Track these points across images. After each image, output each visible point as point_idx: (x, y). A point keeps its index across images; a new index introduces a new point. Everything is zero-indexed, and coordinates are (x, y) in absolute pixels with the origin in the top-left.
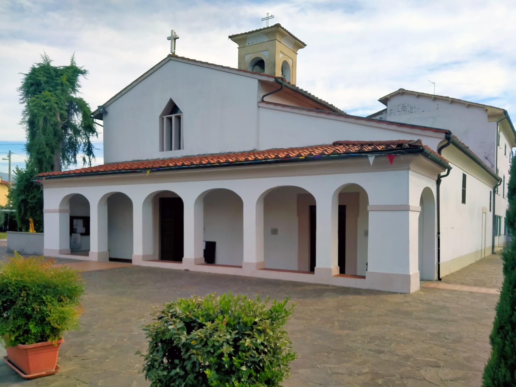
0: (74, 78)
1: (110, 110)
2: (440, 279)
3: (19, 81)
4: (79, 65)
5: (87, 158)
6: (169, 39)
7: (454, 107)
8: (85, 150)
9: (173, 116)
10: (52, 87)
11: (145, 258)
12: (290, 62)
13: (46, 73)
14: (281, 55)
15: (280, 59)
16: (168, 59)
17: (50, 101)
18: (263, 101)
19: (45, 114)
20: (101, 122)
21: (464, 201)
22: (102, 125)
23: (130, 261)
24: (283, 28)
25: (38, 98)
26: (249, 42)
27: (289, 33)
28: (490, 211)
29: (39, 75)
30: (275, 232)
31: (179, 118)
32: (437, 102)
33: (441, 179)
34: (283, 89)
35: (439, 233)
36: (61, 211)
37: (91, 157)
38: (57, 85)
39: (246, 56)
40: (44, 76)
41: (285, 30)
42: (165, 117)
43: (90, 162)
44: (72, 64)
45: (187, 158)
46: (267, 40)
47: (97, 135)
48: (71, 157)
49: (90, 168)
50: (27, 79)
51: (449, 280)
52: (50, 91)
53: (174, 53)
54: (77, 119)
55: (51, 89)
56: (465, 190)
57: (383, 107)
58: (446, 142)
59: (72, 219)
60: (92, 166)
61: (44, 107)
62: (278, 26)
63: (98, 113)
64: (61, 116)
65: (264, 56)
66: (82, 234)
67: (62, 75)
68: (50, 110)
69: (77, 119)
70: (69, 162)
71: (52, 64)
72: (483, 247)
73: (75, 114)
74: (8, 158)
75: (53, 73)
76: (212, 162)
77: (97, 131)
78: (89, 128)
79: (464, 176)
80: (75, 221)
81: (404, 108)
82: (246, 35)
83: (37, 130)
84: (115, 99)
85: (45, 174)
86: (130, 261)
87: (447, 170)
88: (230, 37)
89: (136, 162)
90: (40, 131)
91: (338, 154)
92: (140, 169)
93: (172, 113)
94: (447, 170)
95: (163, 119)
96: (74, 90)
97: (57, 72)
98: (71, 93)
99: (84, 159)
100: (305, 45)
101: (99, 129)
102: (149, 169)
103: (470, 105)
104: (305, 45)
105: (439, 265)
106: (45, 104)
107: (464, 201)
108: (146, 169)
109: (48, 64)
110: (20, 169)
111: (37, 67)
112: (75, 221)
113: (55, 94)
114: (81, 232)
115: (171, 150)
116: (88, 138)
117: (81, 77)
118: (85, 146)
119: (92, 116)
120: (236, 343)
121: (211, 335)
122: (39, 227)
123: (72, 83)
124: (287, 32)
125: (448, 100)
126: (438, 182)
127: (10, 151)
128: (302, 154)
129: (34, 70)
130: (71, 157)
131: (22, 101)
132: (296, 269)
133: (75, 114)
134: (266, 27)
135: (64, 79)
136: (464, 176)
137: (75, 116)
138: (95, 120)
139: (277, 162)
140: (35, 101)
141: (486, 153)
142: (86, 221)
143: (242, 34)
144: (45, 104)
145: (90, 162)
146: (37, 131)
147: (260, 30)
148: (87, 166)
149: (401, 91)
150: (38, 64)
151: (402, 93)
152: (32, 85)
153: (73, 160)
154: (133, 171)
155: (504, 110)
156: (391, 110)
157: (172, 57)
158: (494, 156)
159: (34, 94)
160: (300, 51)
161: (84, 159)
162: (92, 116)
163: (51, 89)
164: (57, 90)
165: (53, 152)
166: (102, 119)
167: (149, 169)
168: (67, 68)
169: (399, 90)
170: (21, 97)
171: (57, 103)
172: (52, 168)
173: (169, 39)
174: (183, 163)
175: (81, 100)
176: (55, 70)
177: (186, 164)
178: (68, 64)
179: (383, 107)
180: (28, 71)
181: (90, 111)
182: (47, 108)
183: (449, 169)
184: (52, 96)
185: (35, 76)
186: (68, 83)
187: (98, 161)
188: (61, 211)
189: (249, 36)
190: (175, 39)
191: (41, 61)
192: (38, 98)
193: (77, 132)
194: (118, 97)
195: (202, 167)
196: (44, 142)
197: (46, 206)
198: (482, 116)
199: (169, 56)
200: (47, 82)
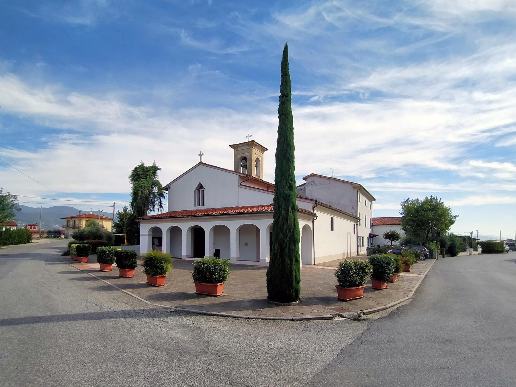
0: (155, 172)
1: (171, 186)
2: (315, 264)
3: (130, 173)
4: (157, 165)
5: (160, 209)
6: (199, 155)
7: (337, 183)
8: (159, 205)
9: (201, 190)
10: (145, 176)
11: (188, 256)
12: (260, 158)
13: (142, 170)
14: (255, 155)
15: (254, 157)
16: (199, 164)
17: (144, 184)
18: (241, 185)
19: (142, 189)
20: (167, 192)
21: (332, 229)
22: (168, 193)
23: (181, 258)
24: (256, 142)
25: (138, 182)
26: (239, 148)
27: (259, 144)
28: (354, 234)
29: (139, 171)
30: (246, 244)
31: (203, 191)
32: (329, 180)
33: (314, 220)
34: (250, 179)
35: (314, 244)
36: (148, 235)
37: (162, 208)
38: (147, 175)
39: (238, 155)
40: (141, 171)
41: (257, 143)
42: (197, 191)
43: (161, 211)
44: (154, 165)
45: (207, 210)
46: (248, 148)
47: (165, 198)
48: (152, 208)
49: (162, 214)
50: (133, 173)
51: (318, 265)
52: (144, 179)
53: (201, 162)
54: (155, 190)
55: (145, 177)
56: (333, 225)
57: (305, 182)
58: (316, 205)
59: (153, 238)
60: (162, 213)
61: (141, 186)
62: (253, 141)
63: (166, 188)
64: (149, 190)
65: (247, 155)
66: (157, 246)
67: (150, 170)
68: (144, 187)
69: (155, 190)
70: (151, 210)
71: (145, 165)
72: (349, 252)
73: (154, 187)
74: (113, 206)
75: (145, 170)
76: (217, 213)
77: (165, 196)
78: (161, 195)
79: (332, 219)
80: (154, 239)
81: (314, 183)
82: (237, 145)
83: (138, 197)
84: (174, 181)
85: (142, 217)
86: (181, 258)
87: (316, 217)
88: (230, 146)
89: (183, 212)
90: (140, 197)
91: (268, 211)
92: (186, 216)
93: (200, 189)
94: (316, 217)
95: (196, 191)
96: (155, 177)
97: (148, 169)
98: (153, 178)
99: (158, 210)
100: (268, 150)
101: (166, 195)
102: (190, 216)
103: (344, 182)
104: (268, 150)
105: (314, 258)
106: (142, 185)
107: (332, 229)
108: (188, 216)
109: (143, 165)
110: (120, 212)
111: (138, 167)
112: (154, 239)
113: (147, 180)
114: (157, 245)
115: (200, 206)
116: (161, 199)
117: (158, 171)
118: (159, 203)
119: (163, 189)
120: (215, 267)
121: (209, 265)
122: (138, 243)
123: (154, 174)
124: (258, 144)
125: (334, 180)
126: (313, 222)
127: (114, 202)
128: (254, 211)
129: (136, 168)
130: (152, 208)
131: (130, 183)
132: (256, 260)
133: (154, 187)
134: (248, 141)
135: (151, 173)
136: (332, 219)
137: (155, 189)
138: (165, 191)
139: (244, 214)
140: (138, 183)
141: (352, 205)
142: (160, 240)
143: (235, 145)
144: (142, 185)
145: (161, 211)
146: (138, 197)
147: (245, 143)
148: (159, 213)
149: (312, 175)
150: (138, 166)
151: (313, 175)
152: (136, 175)
153: (153, 210)
154: (183, 217)
155: (360, 184)
156: (308, 184)
157: (201, 163)
158: (356, 207)
159: (137, 180)
160: (265, 152)
161: (158, 210)
162: (163, 189)
163: (145, 177)
164: (147, 178)
165: (144, 207)
166: (167, 191)
167: (190, 216)
168: (152, 167)
169: (312, 174)
170: (130, 181)
171: (147, 184)
172: (144, 214)
173: (199, 155)
174: (205, 214)
175: (157, 181)
176: (147, 168)
177: (206, 214)
178: (152, 165)
179: (305, 182)
180: (133, 169)
181: (161, 187)
182: (143, 186)
183: (317, 217)
184: (145, 181)
185: (137, 171)
186: (152, 175)
187: (165, 210)
188: (148, 235)
189: (239, 146)
190: (202, 155)
191: (140, 164)
192: (138, 182)
193: (155, 196)
194: (175, 180)
195: (213, 216)
196: (141, 203)
197: (142, 232)
198: (350, 187)
199: (199, 163)
200: (142, 174)
